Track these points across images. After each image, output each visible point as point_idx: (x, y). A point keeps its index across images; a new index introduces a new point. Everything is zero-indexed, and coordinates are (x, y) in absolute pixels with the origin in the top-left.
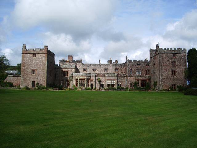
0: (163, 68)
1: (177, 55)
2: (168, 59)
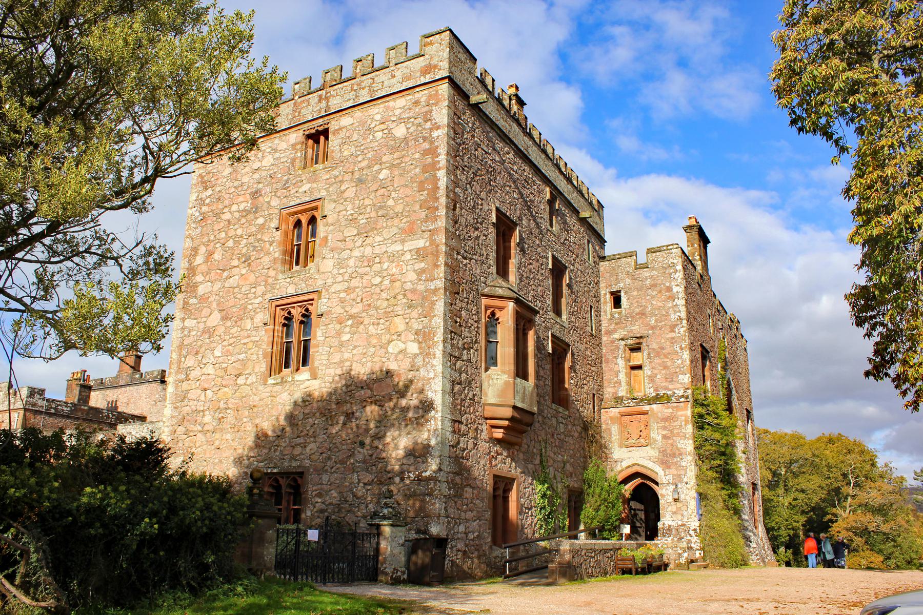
0: (203, 299)
1: (346, 120)
2: (256, 194)
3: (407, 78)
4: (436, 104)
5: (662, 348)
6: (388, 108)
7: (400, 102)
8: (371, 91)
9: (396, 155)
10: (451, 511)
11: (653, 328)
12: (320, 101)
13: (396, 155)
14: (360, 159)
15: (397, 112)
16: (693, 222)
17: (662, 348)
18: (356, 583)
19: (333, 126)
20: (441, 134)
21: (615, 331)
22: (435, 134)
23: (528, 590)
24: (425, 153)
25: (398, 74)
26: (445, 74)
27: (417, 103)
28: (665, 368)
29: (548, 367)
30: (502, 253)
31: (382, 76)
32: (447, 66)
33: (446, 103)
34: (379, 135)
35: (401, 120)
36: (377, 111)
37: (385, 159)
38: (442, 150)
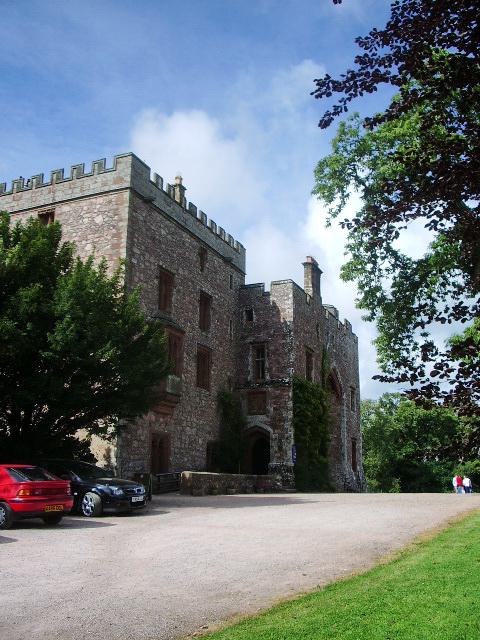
1: (66, 208)
3: (105, 184)
4: (121, 204)
5: (277, 350)
6: (92, 204)
7: (100, 200)
8: (82, 191)
9: (96, 235)
10: (124, 455)
11: (272, 336)
12: (49, 193)
13: (96, 235)
14: (74, 234)
15: (98, 207)
16: (310, 261)
17: (277, 350)
18: (308, 585)
19: (58, 211)
20: (124, 224)
21: (247, 337)
22: (121, 224)
23: (232, 510)
24: (114, 236)
25: (99, 180)
26: (128, 185)
27: (110, 202)
28: (279, 363)
29: (194, 364)
30: (163, 292)
31: (87, 182)
32: (129, 180)
33: (127, 205)
34: (86, 220)
35: (100, 212)
36: (84, 204)
37: (89, 237)
38: (124, 235)
